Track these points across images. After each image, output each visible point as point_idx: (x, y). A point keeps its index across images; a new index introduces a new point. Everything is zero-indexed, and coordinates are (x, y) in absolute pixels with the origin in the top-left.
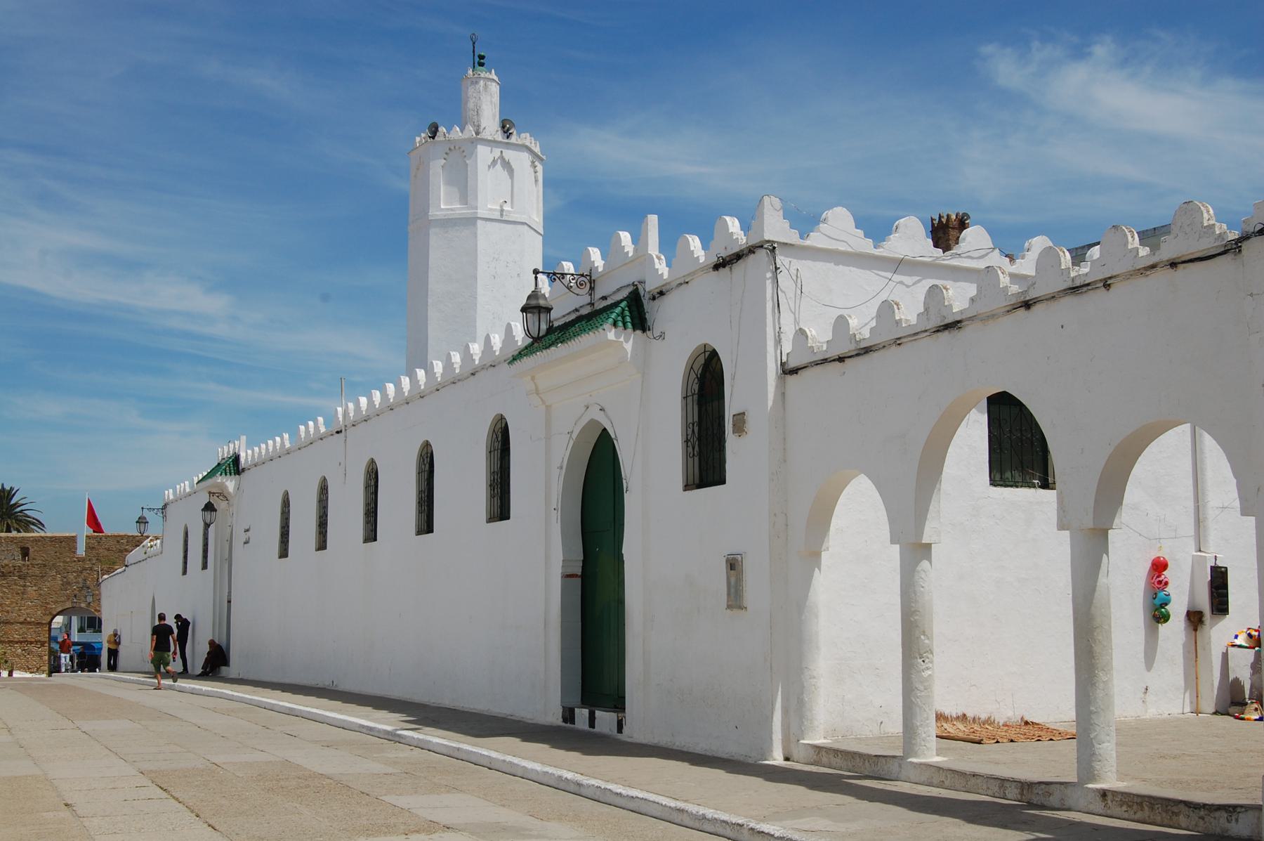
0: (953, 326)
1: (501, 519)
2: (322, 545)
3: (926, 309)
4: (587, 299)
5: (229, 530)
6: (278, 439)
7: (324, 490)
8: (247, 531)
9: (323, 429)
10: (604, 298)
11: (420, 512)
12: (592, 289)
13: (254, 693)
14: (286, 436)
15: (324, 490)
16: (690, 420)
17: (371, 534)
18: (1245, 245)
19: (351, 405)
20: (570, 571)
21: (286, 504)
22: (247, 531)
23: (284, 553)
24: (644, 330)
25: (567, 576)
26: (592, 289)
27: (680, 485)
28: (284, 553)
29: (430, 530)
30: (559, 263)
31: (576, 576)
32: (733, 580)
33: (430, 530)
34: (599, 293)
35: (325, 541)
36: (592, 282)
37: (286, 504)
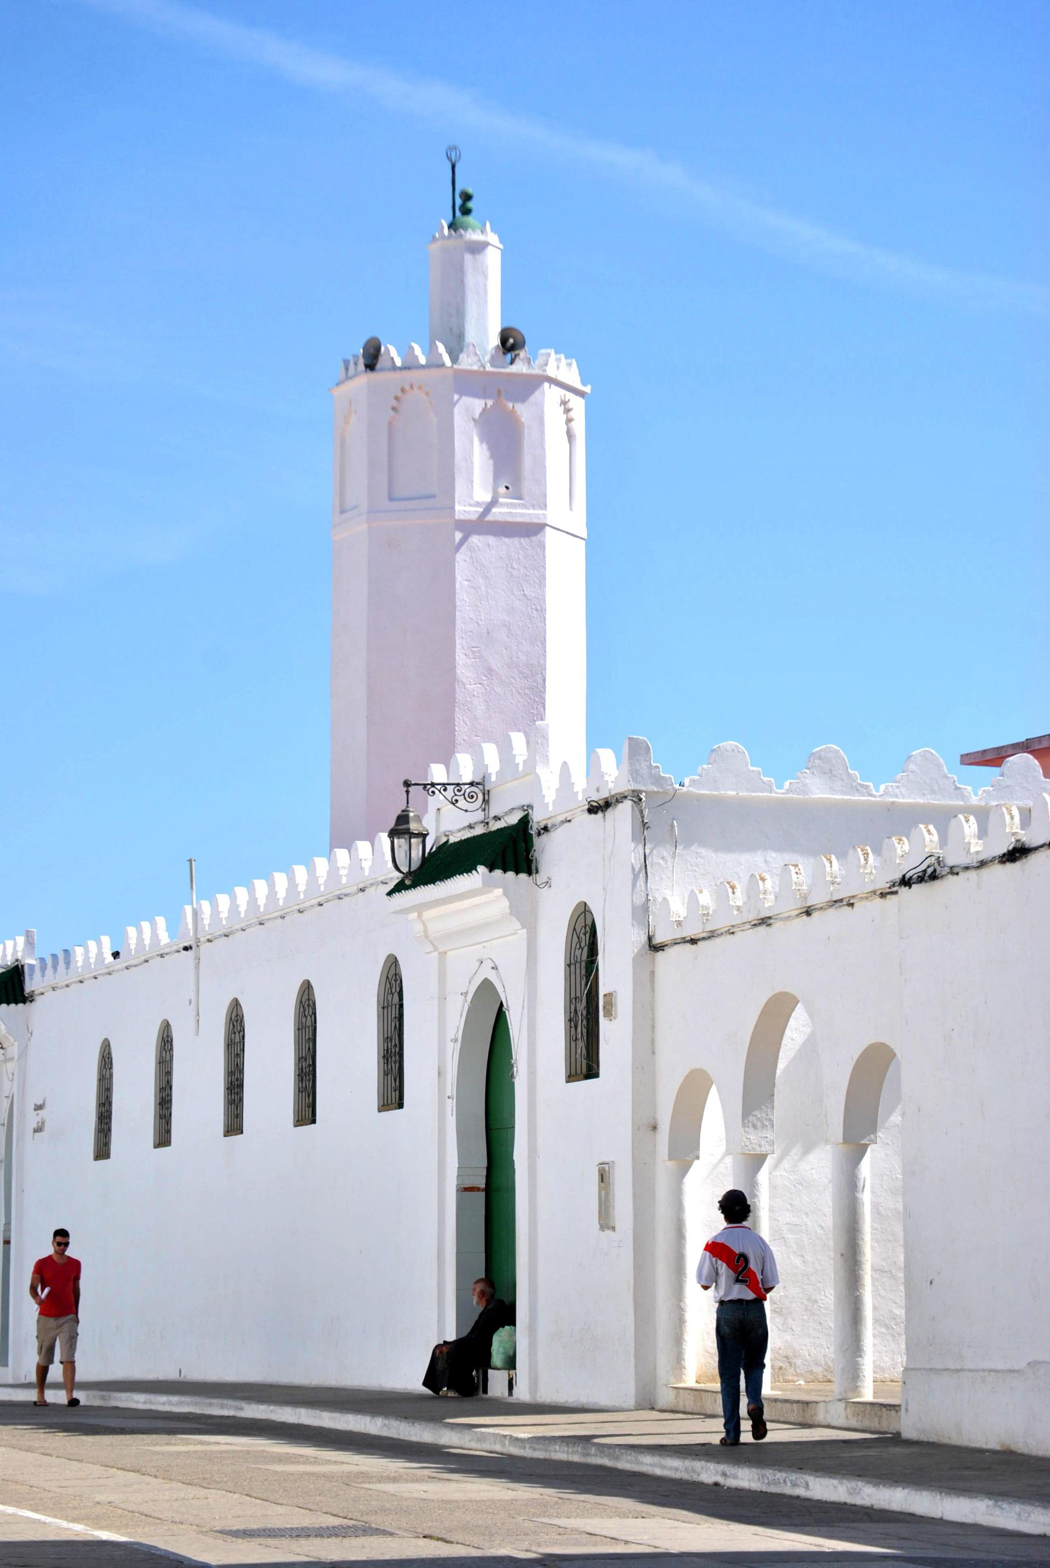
0: (764, 921)
1: (588, 1076)
2: (163, 1138)
3: (749, 898)
4: (480, 816)
5: (6, 1104)
6: (146, 926)
7: (166, 1043)
8: (39, 1108)
9: (164, 939)
10: (497, 818)
11: (571, 1039)
12: (486, 801)
13: (187, 1443)
14: (161, 921)
15: (166, 1043)
16: (573, 996)
17: (234, 1125)
18: (889, 896)
19: (206, 906)
20: (468, 1184)
21: (106, 1061)
22: (39, 1108)
23: (102, 1151)
24: (530, 873)
25: (465, 1190)
26: (486, 801)
27: (92, 1156)
28: (102, 1151)
29: (592, 1072)
30: (426, 770)
31: (478, 1189)
32: (603, 1193)
33: (592, 1072)
34: (495, 810)
35: (168, 1131)
36: (486, 794)
37: (106, 1061)
